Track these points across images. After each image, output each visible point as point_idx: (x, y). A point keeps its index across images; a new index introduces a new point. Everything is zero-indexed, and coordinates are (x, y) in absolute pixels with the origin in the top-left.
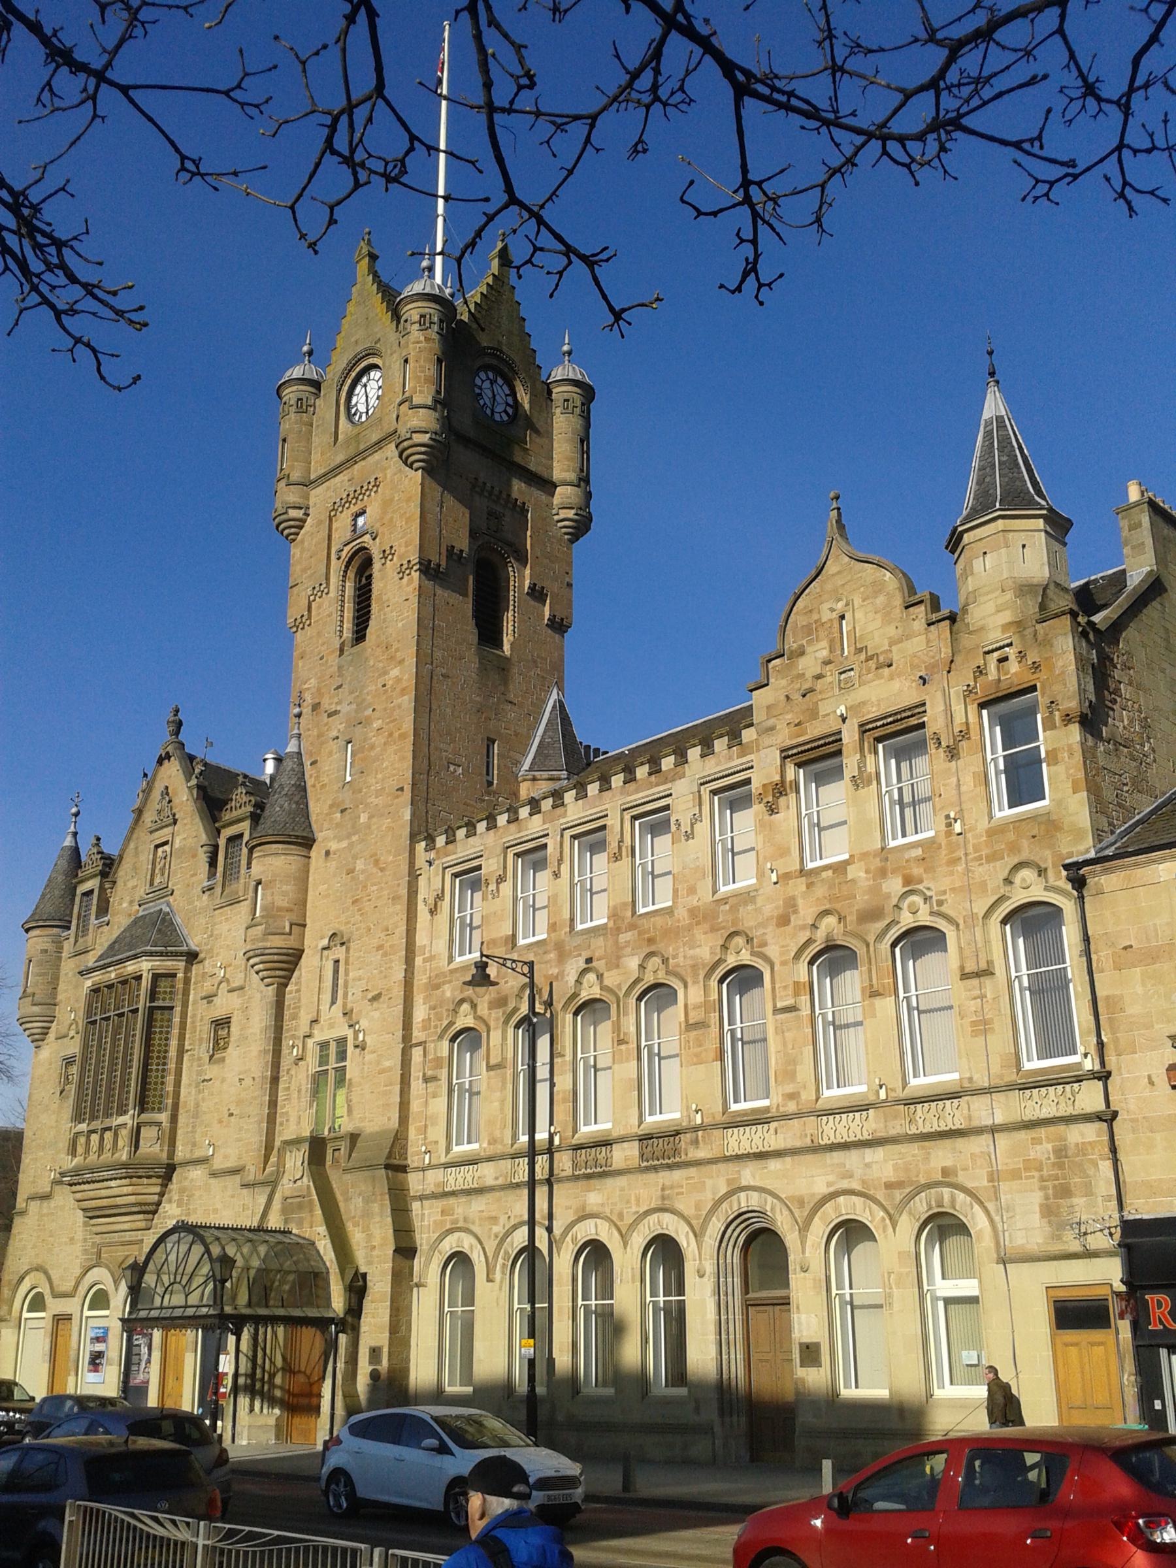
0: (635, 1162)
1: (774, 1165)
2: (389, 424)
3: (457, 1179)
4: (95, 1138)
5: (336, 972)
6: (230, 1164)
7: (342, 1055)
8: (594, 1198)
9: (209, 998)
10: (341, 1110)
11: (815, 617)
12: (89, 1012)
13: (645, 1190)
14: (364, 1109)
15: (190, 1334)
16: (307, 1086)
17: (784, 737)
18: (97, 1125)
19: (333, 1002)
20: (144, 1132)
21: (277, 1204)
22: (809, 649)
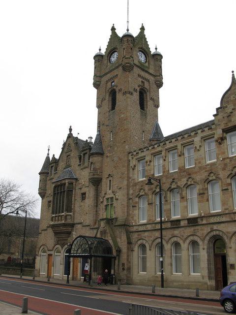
0: (186, 225)
1: (223, 225)
2: (120, 62)
3: (141, 229)
4: (57, 218)
5: (110, 182)
6: (87, 224)
7: (112, 201)
8: (176, 232)
9: (81, 189)
10: (113, 213)
11: (230, 98)
12: (54, 191)
13: (189, 231)
14: (119, 212)
15: (79, 259)
16: (104, 207)
17: (223, 127)
18: (57, 215)
19: (110, 189)
20: (68, 217)
21: (99, 233)
22: (228, 106)
